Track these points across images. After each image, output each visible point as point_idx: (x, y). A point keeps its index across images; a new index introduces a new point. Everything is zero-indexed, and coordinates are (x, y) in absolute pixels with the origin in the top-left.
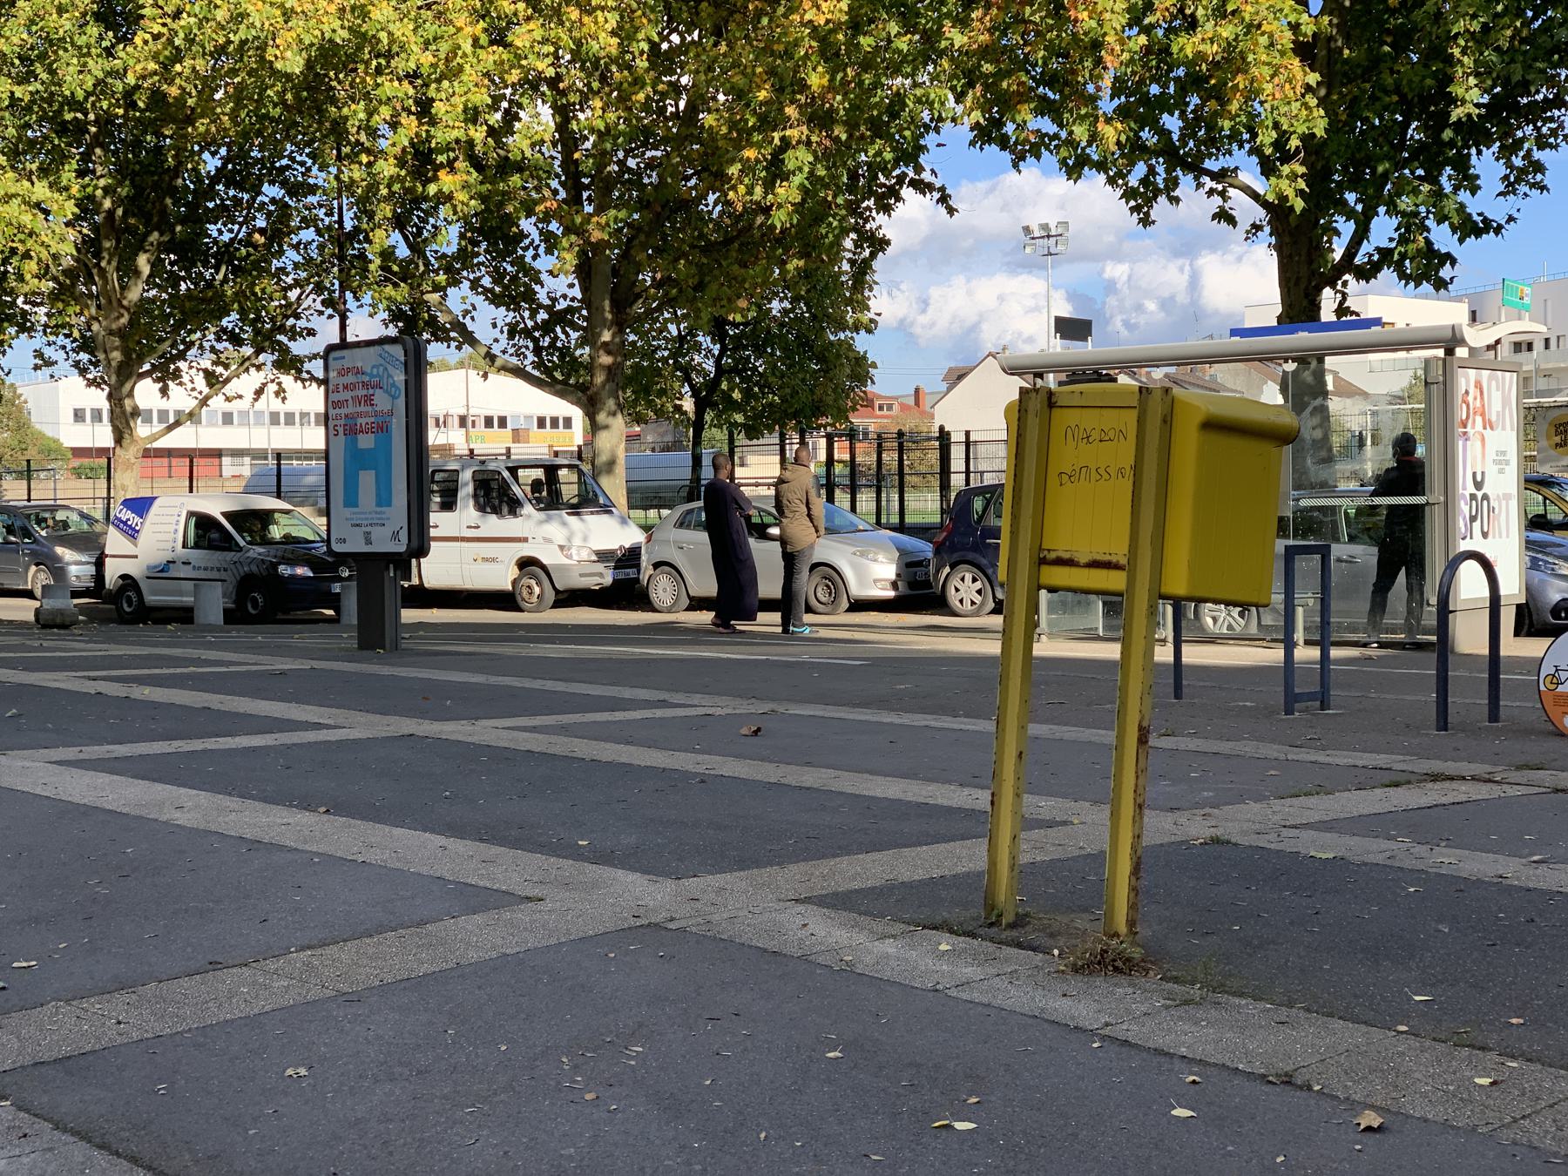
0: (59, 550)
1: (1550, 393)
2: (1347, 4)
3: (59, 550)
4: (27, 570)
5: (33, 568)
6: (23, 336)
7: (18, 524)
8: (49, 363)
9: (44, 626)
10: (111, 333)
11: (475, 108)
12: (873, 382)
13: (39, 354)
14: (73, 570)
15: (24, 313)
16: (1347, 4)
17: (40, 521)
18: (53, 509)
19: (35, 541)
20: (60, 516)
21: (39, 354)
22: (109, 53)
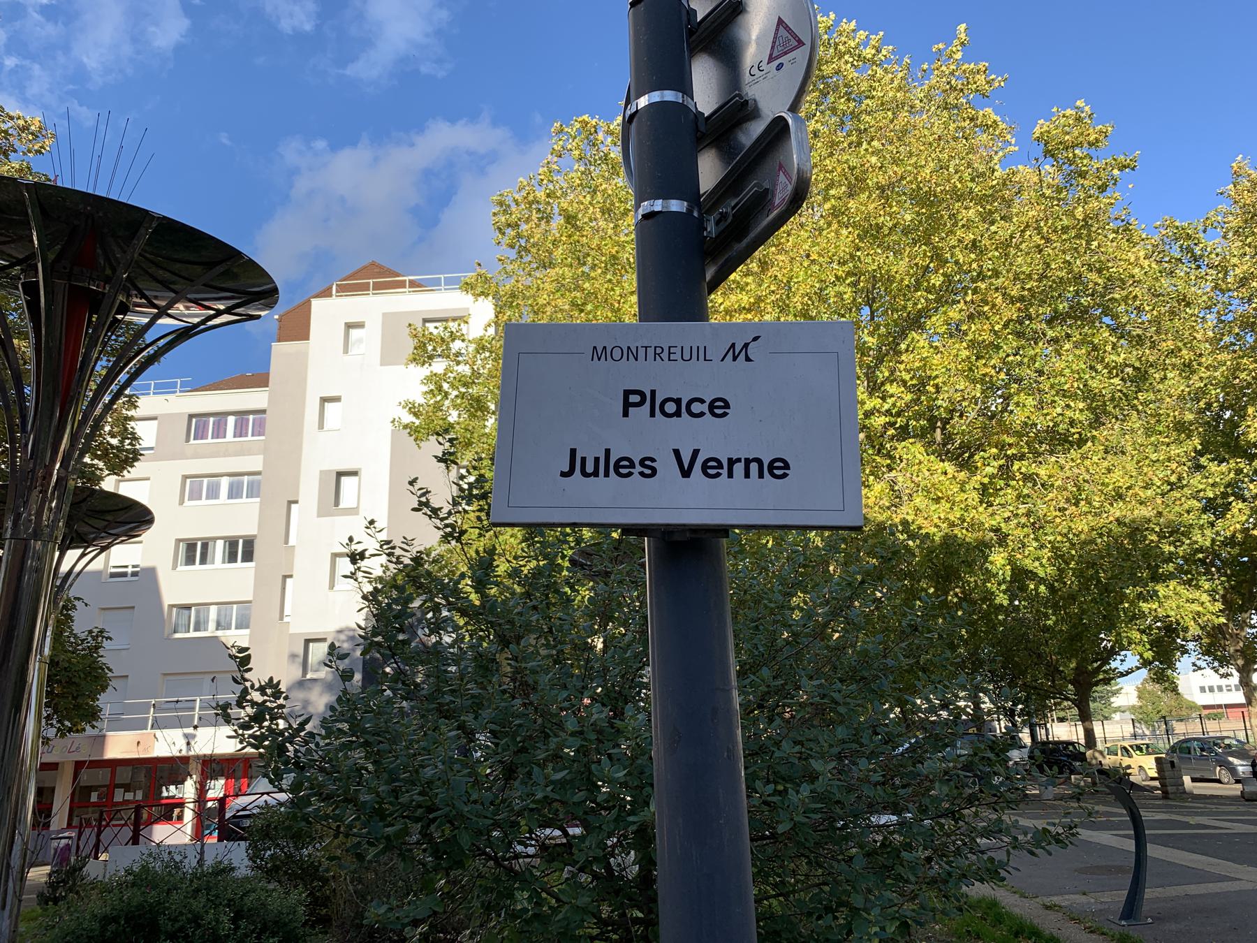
0: (1231, 759)
1: (735, 618)
2: (1254, 284)
3: (1231, 759)
4: (1215, 769)
5: (1218, 768)
6: (1186, 656)
7: (1206, 747)
8: (1200, 668)
9: (1247, 800)
10: (1237, 651)
11: (1000, 546)
12: (110, 670)
13: (1194, 664)
14: (1240, 769)
15: (1183, 646)
16: (1254, 284)
17: (1216, 744)
18: (1223, 738)
19: (1216, 754)
20: (1227, 742)
21: (1194, 664)
22: (1212, 525)
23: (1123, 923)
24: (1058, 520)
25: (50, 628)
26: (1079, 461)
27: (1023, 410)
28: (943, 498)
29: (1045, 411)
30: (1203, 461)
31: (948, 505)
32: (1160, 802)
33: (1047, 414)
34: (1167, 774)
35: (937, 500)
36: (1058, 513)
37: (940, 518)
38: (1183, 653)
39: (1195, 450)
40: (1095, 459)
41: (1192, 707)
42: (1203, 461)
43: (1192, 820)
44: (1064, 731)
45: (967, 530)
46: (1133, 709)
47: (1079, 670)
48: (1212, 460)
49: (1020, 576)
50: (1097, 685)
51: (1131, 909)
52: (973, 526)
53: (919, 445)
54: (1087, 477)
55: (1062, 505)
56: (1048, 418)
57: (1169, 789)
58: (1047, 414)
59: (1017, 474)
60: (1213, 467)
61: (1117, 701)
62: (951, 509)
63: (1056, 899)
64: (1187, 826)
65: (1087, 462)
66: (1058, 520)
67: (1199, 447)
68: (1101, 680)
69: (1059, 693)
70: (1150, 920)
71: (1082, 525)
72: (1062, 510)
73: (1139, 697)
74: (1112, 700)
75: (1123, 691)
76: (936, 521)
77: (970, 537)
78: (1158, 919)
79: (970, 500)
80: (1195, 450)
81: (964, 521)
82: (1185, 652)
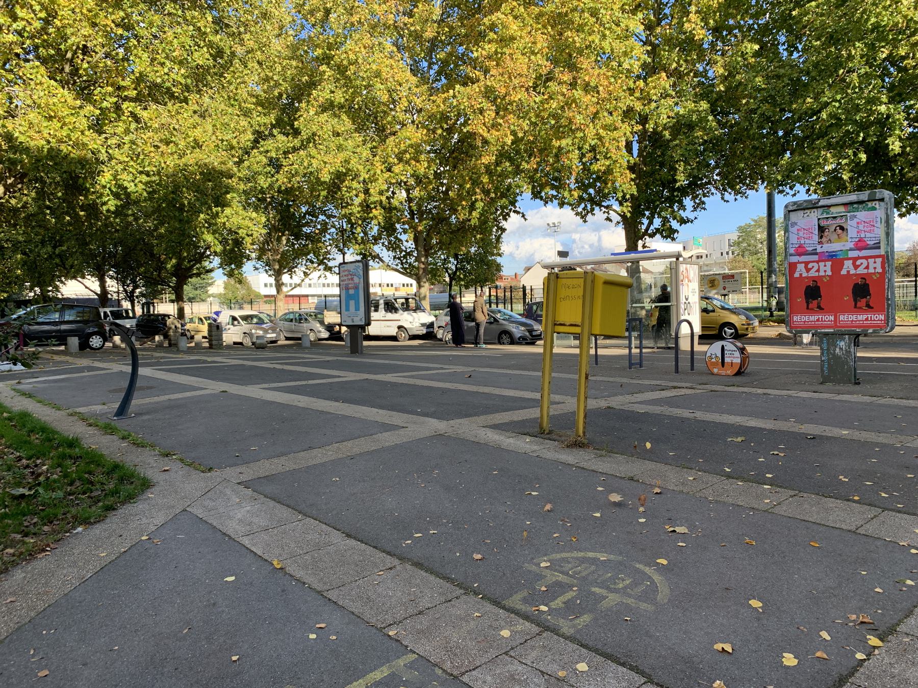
23: (115, 418)
24: (152, 154)
25: (53, 328)
26: (173, 113)
27: (140, 63)
28: (55, 117)
29: (155, 69)
30: (275, 131)
31: (59, 125)
32: (208, 350)
33: (157, 71)
34: (213, 333)
35: (50, 118)
36: (153, 149)
37: (49, 134)
38: (248, 259)
39: (271, 124)
40: (185, 115)
41: (258, 296)
42: (275, 131)
43: (209, 359)
44: (165, 308)
45: (73, 147)
46: (219, 296)
47: (178, 267)
48: (280, 133)
49: (121, 192)
50: (191, 278)
51: (122, 411)
52: (76, 145)
53: (42, 70)
54: (177, 127)
55: (156, 143)
56: (157, 74)
57: (214, 342)
58: (157, 71)
59: (126, 111)
60: (281, 138)
61: (212, 290)
62: (62, 128)
63: (78, 410)
64: (205, 362)
65: (179, 117)
66: (152, 154)
67: (274, 122)
68: (194, 274)
69: (163, 282)
70: (133, 415)
71: (171, 162)
72: (157, 147)
73: (225, 288)
74: (209, 288)
75: (216, 283)
76: (46, 135)
77: (75, 153)
78: (138, 414)
79: (77, 123)
80: (271, 124)
81: (70, 140)
82: (249, 258)
